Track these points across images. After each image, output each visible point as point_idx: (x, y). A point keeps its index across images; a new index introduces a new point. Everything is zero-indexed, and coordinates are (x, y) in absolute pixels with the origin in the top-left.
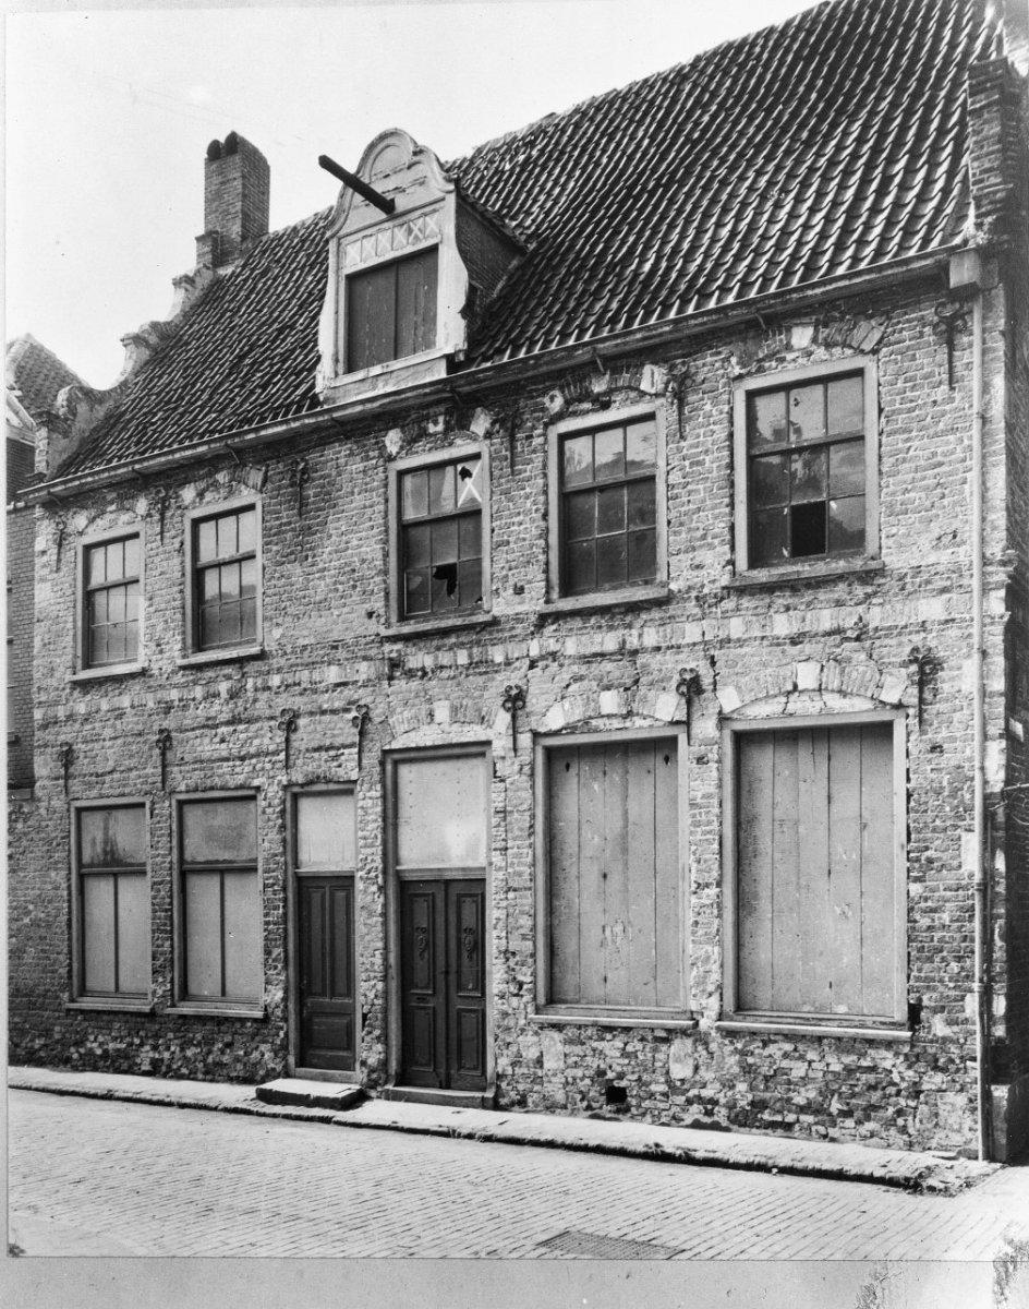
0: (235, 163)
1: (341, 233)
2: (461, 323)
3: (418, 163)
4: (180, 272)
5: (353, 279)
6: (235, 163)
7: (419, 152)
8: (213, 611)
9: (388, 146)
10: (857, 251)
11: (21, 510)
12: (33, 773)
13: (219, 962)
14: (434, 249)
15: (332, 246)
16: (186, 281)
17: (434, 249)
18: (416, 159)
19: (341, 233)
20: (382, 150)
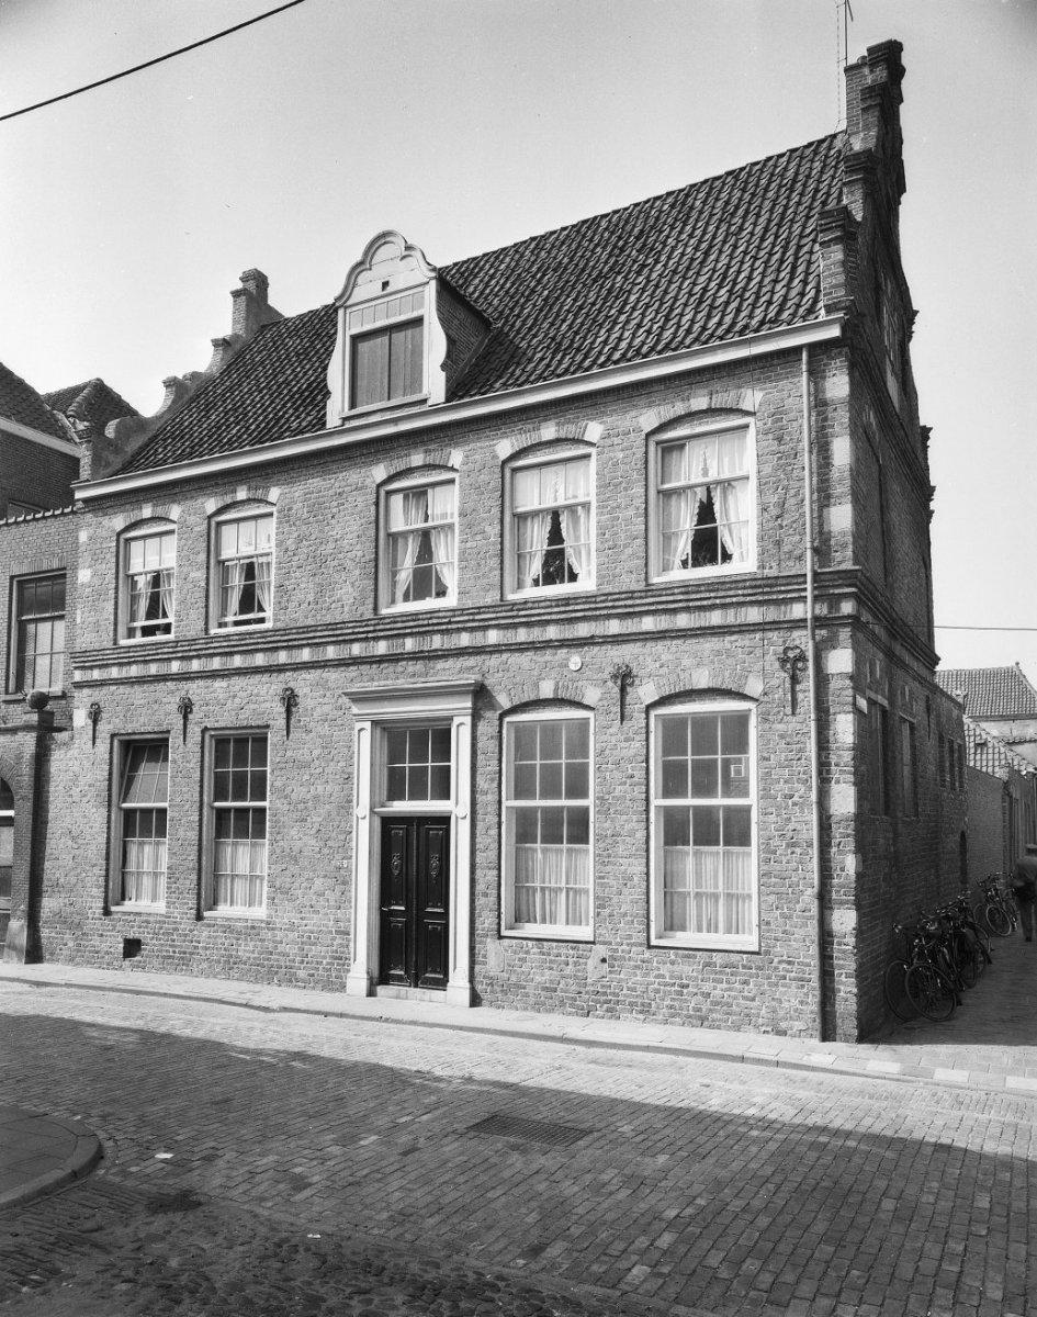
0: (254, 290)
1: (349, 303)
2: (443, 375)
3: (410, 256)
4: (220, 335)
5: (356, 339)
6: (254, 290)
7: (408, 248)
8: (492, 306)
9: (385, 243)
10: (808, 268)
11: (38, 520)
12: (851, 375)
13: (49, 642)
14: (418, 321)
15: (341, 312)
16: (222, 344)
17: (418, 321)
18: (407, 253)
19: (349, 303)
20: (378, 248)
